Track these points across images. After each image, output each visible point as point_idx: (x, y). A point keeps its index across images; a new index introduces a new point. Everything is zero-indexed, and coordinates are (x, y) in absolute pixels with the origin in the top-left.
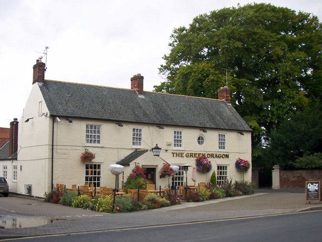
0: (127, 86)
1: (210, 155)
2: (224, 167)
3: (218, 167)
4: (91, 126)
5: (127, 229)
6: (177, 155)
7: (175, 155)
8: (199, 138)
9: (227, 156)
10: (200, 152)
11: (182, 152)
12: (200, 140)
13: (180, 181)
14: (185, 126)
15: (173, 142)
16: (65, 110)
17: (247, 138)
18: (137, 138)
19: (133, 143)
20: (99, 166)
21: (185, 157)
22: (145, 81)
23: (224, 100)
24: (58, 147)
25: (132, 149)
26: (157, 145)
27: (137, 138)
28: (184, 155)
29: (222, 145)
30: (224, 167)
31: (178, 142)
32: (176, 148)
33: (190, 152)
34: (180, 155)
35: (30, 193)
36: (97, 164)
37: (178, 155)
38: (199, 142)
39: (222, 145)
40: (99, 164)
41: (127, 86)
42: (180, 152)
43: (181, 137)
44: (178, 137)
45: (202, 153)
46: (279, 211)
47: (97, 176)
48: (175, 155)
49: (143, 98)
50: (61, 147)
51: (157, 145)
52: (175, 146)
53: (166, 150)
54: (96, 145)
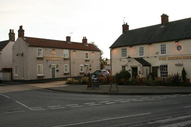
0: (65, 40)
3: (122, 66)
4: (163, 45)
8: (178, 47)
12: (179, 48)
13: (166, 74)
14: (135, 45)
15: (160, 51)
19: (122, 56)
20: (167, 66)
22: (129, 27)
24: (113, 61)
26: (129, 56)
28: (167, 58)
31: (163, 51)
33: (171, 57)
34: (164, 59)
38: (178, 49)
40: (167, 65)
41: (65, 40)
43: (165, 48)
44: (163, 48)
46: (21, 90)
48: (161, 59)
50: (114, 60)
51: (129, 56)
52: (162, 54)
53: (155, 57)
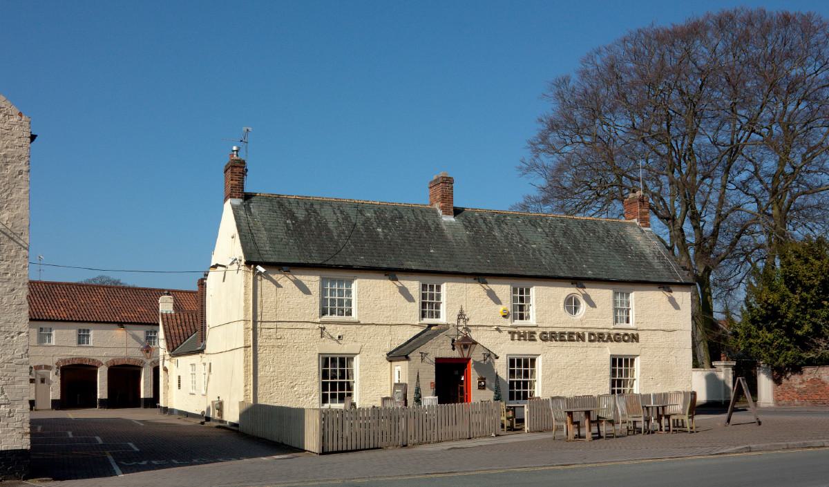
1: (593, 334)
2: (626, 360)
5: (471, 473)
6: (520, 336)
7: (516, 336)
9: (635, 338)
10: (572, 330)
11: (534, 329)
12: (571, 305)
16: (507, 296)
17: (684, 298)
18: (429, 306)
21: (539, 341)
23: (635, 220)
25: (420, 325)
27: (429, 306)
28: (537, 337)
29: (621, 312)
30: (526, 360)
32: (518, 322)
33: (548, 330)
35: (222, 415)
36: (522, 358)
37: (522, 337)
39: (621, 312)
42: (527, 330)
45: (576, 331)
47: (346, 380)
48: (516, 336)
49: (451, 222)
54: (345, 318)
